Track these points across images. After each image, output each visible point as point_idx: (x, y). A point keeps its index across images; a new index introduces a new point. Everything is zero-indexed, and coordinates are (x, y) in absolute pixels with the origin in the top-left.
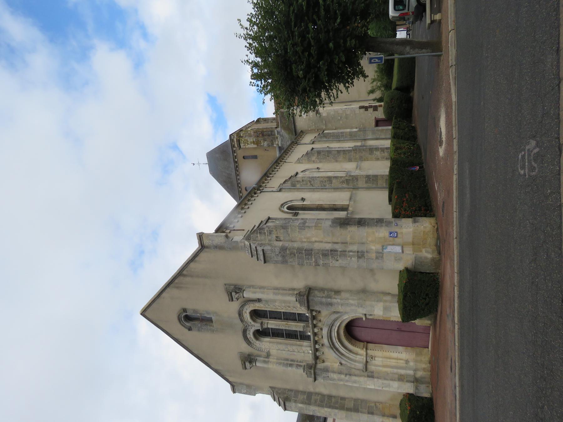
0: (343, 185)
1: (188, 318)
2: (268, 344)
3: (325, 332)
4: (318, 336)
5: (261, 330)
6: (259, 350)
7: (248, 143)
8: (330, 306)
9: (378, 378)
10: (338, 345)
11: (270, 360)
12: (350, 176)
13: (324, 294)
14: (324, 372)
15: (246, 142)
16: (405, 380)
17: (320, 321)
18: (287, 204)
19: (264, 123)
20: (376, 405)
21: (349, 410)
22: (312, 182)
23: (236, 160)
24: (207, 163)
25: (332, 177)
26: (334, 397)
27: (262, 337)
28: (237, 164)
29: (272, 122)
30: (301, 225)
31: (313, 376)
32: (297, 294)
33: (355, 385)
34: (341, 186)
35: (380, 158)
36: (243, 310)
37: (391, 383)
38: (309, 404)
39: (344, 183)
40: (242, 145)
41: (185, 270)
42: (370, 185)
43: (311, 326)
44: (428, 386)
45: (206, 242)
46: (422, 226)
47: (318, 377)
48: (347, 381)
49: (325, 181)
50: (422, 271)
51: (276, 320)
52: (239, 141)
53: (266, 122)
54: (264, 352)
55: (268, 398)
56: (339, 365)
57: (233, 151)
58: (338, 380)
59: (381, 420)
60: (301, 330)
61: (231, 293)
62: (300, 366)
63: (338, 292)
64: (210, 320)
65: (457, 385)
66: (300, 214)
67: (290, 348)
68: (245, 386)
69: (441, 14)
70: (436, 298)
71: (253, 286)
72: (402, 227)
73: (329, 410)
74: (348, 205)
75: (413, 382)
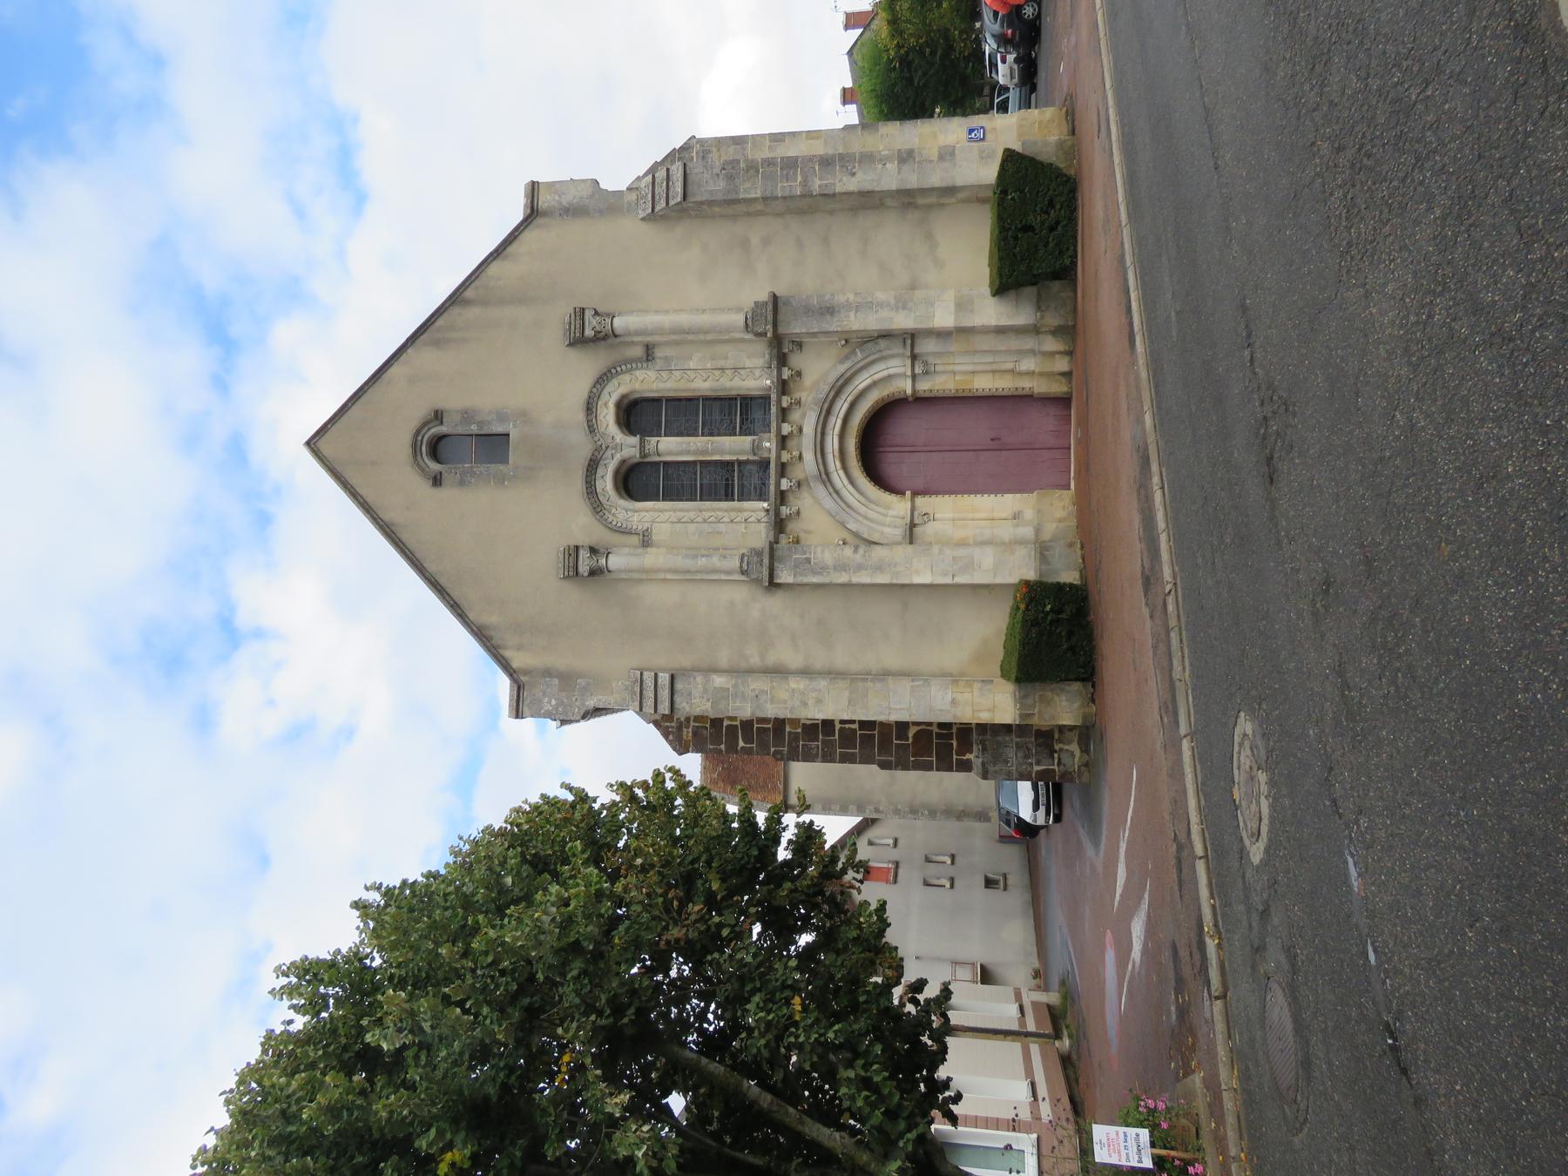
8: (828, 317)
41: (473, 285)
45: (545, 200)
48: (860, 568)
59: (949, 697)
68: (556, 681)
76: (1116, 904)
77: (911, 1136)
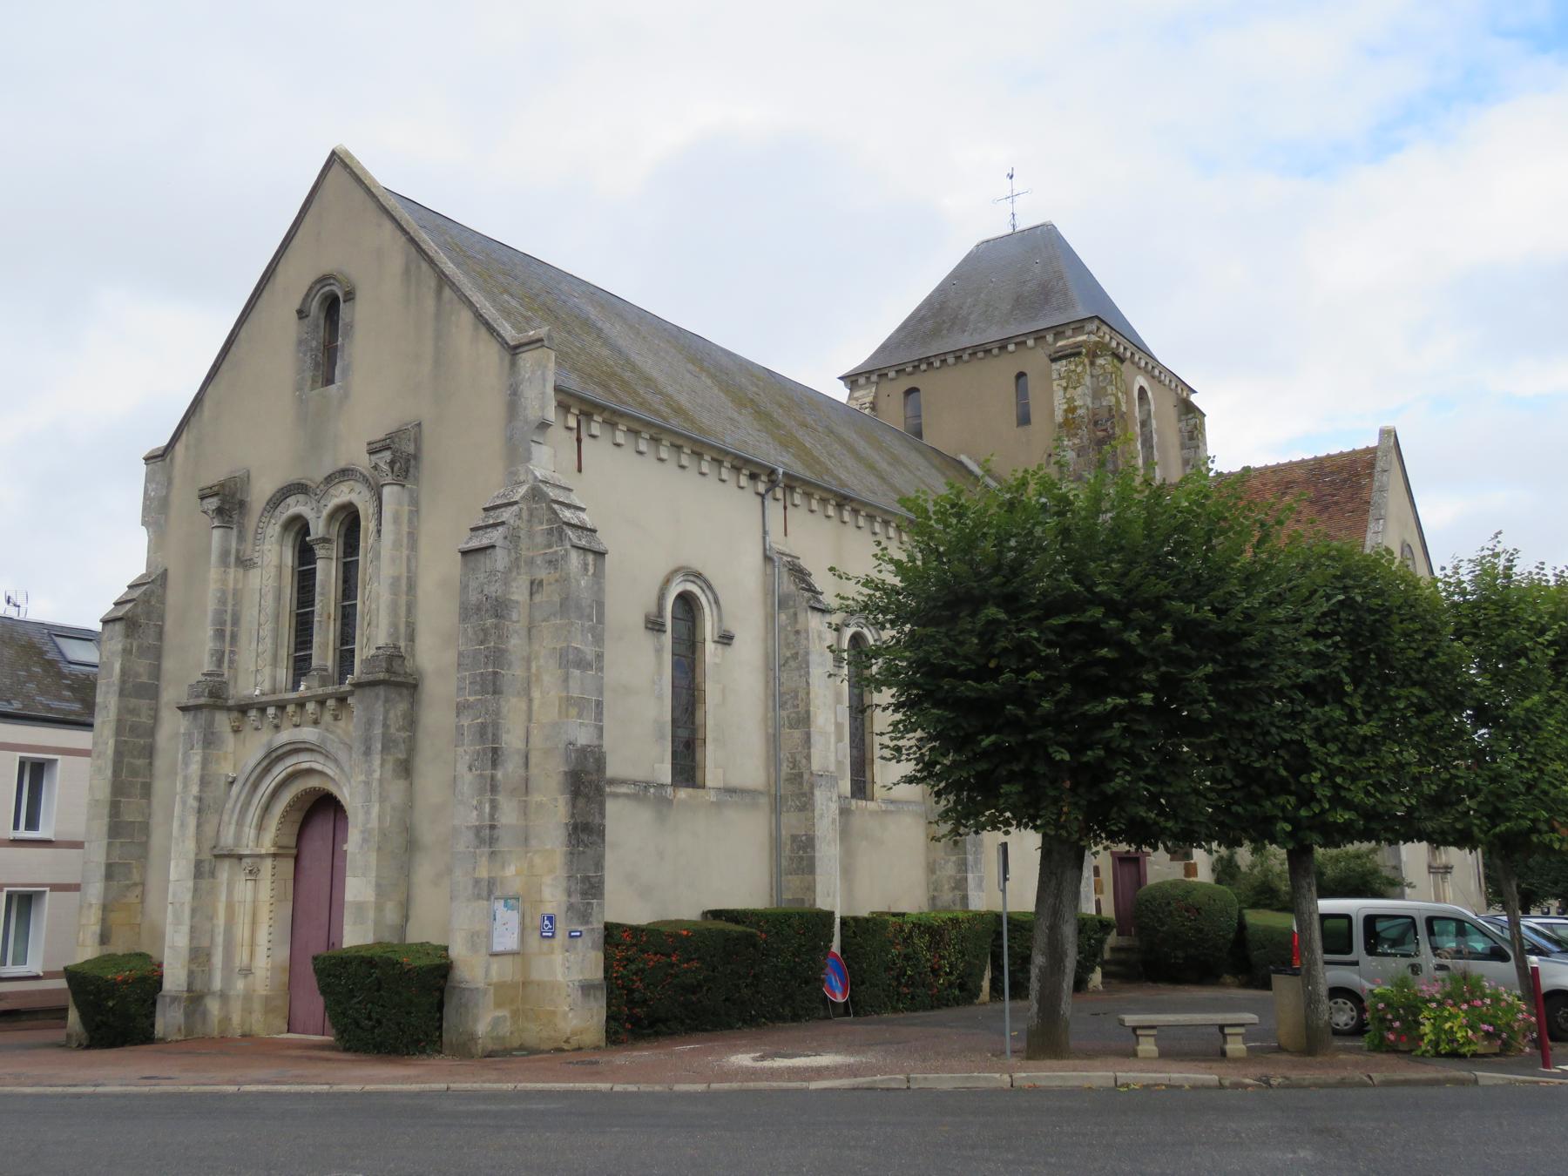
0: (785, 765)
1: (332, 306)
2: (275, 561)
3: (308, 734)
4: (299, 714)
5: (308, 539)
6: (259, 536)
7: (1070, 391)
9: (196, 890)
10: (280, 771)
11: (232, 571)
12: (812, 787)
13: (398, 730)
14: (205, 735)
15: (1071, 382)
16: (194, 967)
17: (336, 718)
18: (703, 591)
19: (1180, 431)
20: (135, 885)
21: (115, 808)
22: (793, 664)
23: (1011, 347)
24: (1017, 230)
25: (809, 728)
26: (151, 764)
27: (295, 540)
28: (995, 351)
29: (1186, 462)
30: (571, 657)
31: (192, 702)
32: (396, 647)
33: (176, 824)
34: (782, 756)
35: (935, 877)
36: (356, 481)
37: (185, 929)
38: (122, 693)
39: (791, 765)
40: (1061, 366)
42: (787, 851)
43: (320, 691)
44: (179, 1030)
46: (567, 1009)
47: (190, 716)
48: (184, 803)
49: (797, 706)
50: (445, 1010)
51: (340, 582)
52: (1073, 354)
53: (1187, 441)
54: (254, 550)
55: (136, 567)
56: (227, 776)
57: (1041, 334)
58: (185, 777)
59: (94, 901)
60: (315, 662)
61: (388, 448)
62: (220, 662)
63: (406, 769)
64: (329, 380)
65: (100, 1089)
66: (658, 638)
67: (267, 630)
68: (164, 493)
69: (1155, 1058)
70: (375, 1047)
71: (417, 511)
72: (567, 951)
73: (110, 751)
74: (703, 787)
75: (189, 990)
76: (850, 1060)
77: (1425, 770)
